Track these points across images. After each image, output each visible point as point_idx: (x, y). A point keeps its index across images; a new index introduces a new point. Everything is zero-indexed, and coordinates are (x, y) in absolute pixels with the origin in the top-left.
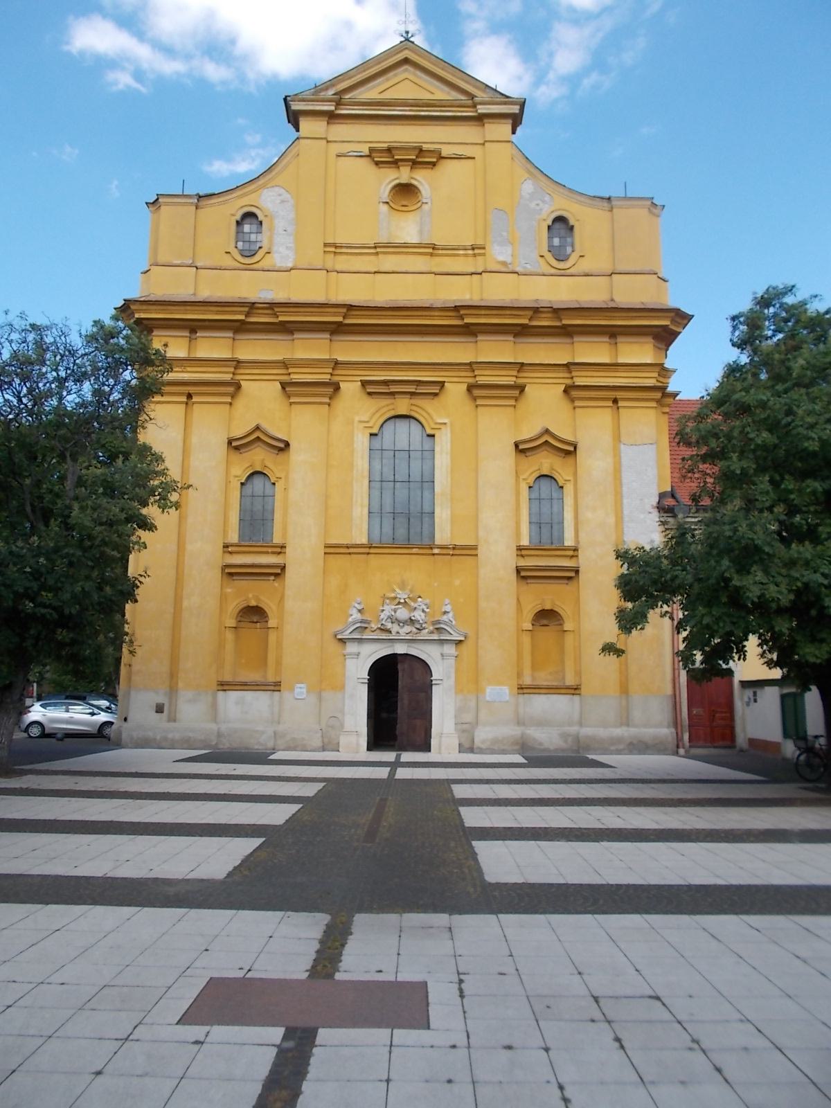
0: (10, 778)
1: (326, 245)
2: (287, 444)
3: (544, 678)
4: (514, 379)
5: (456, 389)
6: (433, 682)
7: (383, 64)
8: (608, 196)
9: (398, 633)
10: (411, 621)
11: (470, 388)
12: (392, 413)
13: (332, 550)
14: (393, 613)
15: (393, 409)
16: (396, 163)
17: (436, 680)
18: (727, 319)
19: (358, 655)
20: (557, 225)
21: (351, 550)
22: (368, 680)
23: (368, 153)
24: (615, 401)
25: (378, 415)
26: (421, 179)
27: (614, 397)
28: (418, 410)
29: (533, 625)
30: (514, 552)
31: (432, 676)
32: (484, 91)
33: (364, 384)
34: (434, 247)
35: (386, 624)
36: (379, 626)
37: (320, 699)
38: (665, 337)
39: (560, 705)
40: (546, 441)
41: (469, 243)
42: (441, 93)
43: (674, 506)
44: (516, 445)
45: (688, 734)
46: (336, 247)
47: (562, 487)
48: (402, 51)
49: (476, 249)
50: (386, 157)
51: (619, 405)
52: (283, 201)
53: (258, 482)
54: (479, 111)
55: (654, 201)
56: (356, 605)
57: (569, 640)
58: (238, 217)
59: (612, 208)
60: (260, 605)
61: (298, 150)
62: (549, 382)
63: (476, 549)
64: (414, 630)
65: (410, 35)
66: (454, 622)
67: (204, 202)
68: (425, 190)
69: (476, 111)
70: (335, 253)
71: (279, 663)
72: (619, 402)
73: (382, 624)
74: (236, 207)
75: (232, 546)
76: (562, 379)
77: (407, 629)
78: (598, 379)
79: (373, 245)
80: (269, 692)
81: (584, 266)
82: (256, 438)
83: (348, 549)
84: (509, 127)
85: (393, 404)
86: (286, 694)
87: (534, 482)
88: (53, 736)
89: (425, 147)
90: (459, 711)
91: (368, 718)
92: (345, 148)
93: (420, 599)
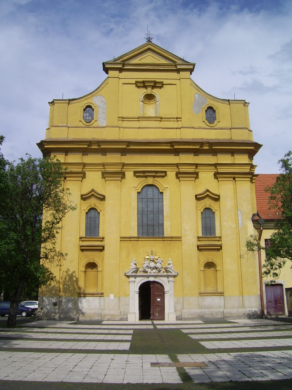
1: (119, 118)
6: (165, 292)
9: (150, 272)
12: (146, 184)
15: (147, 182)
16: (146, 87)
21: (131, 239)
22: (139, 292)
25: (141, 184)
26: (156, 92)
31: (164, 290)
33: (135, 172)
42: (163, 61)
48: (147, 46)
51: (236, 180)
52: (102, 101)
54: (178, 68)
55: (245, 101)
58: (84, 107)
63: (181, 238)
64: (157, 271)
65: (150, 39)
66: (173, 268)
67: (71, 102)
68: (158, 97)
69: (177, 68)
77: (155, 271)
81: (219, 125)
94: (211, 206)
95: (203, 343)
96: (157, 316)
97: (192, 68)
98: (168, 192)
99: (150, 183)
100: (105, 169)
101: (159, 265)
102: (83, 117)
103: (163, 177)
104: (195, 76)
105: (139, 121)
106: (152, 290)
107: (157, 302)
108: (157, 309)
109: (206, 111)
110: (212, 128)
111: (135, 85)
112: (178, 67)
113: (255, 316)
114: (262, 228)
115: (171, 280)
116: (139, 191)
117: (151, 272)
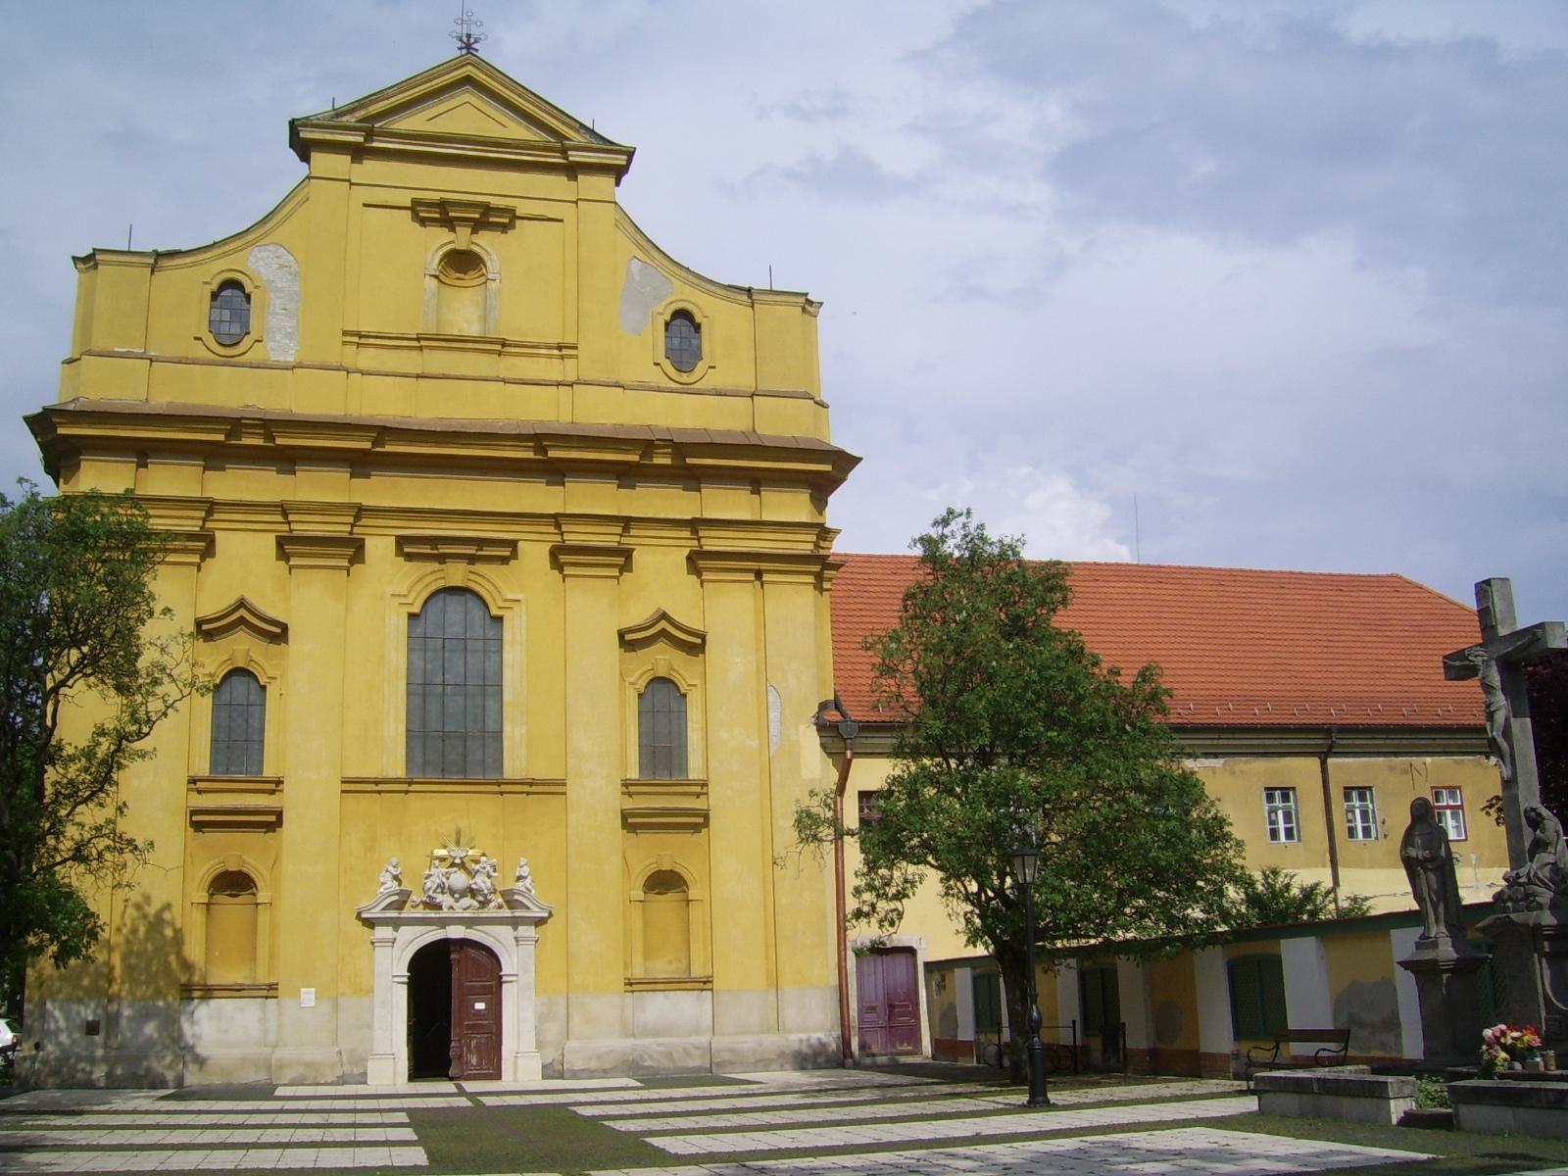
0: (409, 1059)
1: (345, 333)
2: (285, 628)
3: (662, 968)
4: (617, 538)
5: (535, 552)
6: (505, 979)
7: (434, 82)
8: (747, 286)
9: (451, 908)
10: (472, 892)
11: (281, 542)
12: (441, 584)
13: (353, 786)
14: (444, 880)
15: (444, 578)
16: (449, 223)
17: (507, 975)
18: (167, 611)
19: (393, 943)
20: (678, 322)
21: (381, 787)
22: (409, 978)
23: (409, 204)
24: (759, 574)
25: (421, 585)
26: (486, 243)
27: (758, 566)
28: (478, 579)
29: (645, 892)
30: (619, 788)
31: (501, 970)
32: (577, 131)
33: (401, 541)
34: (504, 343)
35: (435, 895)
36: (424, 899)
37: (336, 1007)
38: (822, 488)
39: (683, 1008)
40: (663, 629)
41: (555, 340)
42: (518, 131)
43: (837, 722)
44: (621, 634)
45: (857, 1038)
46: (361, 336)
47: (500, 619)
48: (463, 66)
49: (563, 349)
50: (438, 213)
51: (764, 579)
52: (281, 266)
53: (239, 684)
54: (571, 159)
55: (809, 297)
56: (390, 868)
57: (696, 913)
58: (215, 287)
59: (753, 303)
60: (244, 870)
61: (308, 193)
62: (758, 1115)
63: (565, 784)
64: (475, 903)
65: (472, 40)
66: (533, 892)
67: (164, 263)
68: (493, 263)
69: (567, 159)
70: (358, 344)
71: (273, 956)
72: (764, 575)
73: (429, 896)
74: (215, 270)
75: (200, 780)
76: (684, 538)
77: (467, 901)
78: (735, 543)
79: (415, 336)
80: (260, 1000)
81: (714, 380)
82: (241, 618)
83: (376, 785)
84: (613, 180)
85: (442, 570)
86: (287, 1002)
87: (646, 687)
88: (1462, 673)
89: (495, 202)
90: (543, 1018)
91: (409, 1035)
92: (381, 196)
93: (484, 859)
94: (672, 672)
95: (656, 1141)
96: (472, 1065)
97: (624, 163)
98: (521, 617)
99: (458, 582)
100: (289, 523)
101: (484, 883)
102: (210, 321)
103: (504, 560)
104: (630, 192)
105: (422, 350)
106: (455, 970)
107: (474, 1015)
108: (474, 1042)
109: (667, 324)
110: (687, 390)
111: (409, 212)
112: (573, 156)
113: (821, 1060)
114: (849, 753)
115: (526, 934)
116: (416, 609)
117: (455, 905)
